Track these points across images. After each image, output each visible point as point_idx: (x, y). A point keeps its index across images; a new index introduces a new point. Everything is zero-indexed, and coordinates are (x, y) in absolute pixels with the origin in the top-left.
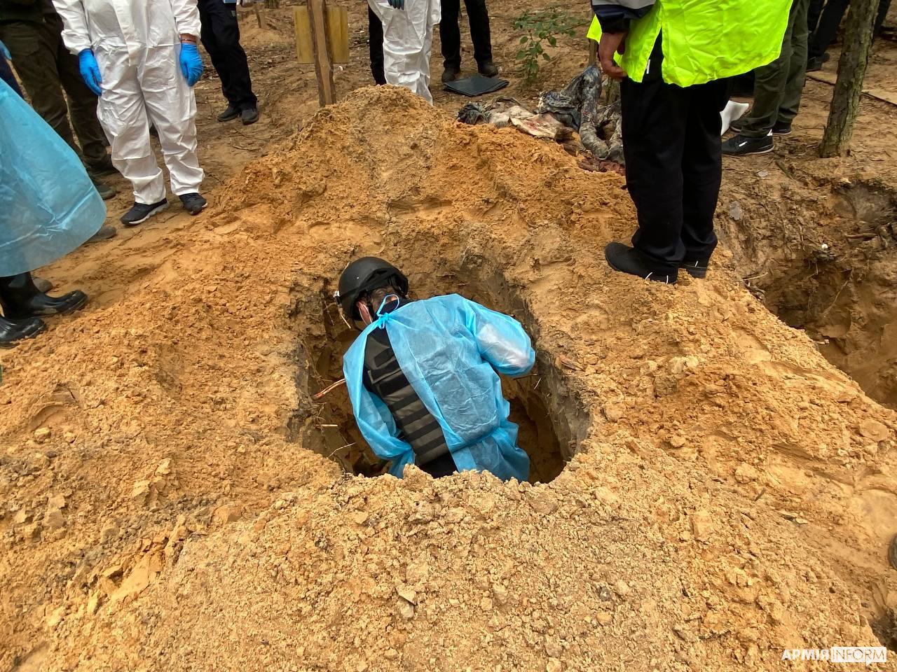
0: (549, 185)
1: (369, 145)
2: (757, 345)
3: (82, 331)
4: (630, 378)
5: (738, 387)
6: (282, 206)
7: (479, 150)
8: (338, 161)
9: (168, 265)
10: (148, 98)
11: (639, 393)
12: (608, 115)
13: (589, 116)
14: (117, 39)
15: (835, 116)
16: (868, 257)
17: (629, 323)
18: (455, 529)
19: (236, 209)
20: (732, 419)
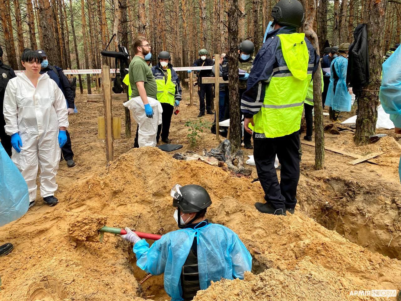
0: (226, 182)
1: (143, 170)
2: (323, 236)
3: (30, 258)
4: (284, 253)
5: (328, 247)
6: (104, 198)
7: (192, 170)
8: (129, 177)
9: (55, 227)
10: (40, 153)
11: (289, 258)
12: (235, 157)
13: (229, 157)
14: (34, 129)
15: (318, 155)
16: (343, 205)
17: (276, 232)
18: (274, 288)
19: (84, 200)
20: (329, 260)
